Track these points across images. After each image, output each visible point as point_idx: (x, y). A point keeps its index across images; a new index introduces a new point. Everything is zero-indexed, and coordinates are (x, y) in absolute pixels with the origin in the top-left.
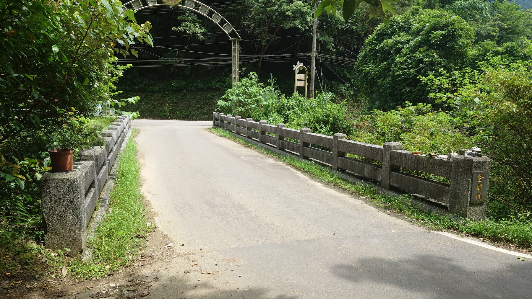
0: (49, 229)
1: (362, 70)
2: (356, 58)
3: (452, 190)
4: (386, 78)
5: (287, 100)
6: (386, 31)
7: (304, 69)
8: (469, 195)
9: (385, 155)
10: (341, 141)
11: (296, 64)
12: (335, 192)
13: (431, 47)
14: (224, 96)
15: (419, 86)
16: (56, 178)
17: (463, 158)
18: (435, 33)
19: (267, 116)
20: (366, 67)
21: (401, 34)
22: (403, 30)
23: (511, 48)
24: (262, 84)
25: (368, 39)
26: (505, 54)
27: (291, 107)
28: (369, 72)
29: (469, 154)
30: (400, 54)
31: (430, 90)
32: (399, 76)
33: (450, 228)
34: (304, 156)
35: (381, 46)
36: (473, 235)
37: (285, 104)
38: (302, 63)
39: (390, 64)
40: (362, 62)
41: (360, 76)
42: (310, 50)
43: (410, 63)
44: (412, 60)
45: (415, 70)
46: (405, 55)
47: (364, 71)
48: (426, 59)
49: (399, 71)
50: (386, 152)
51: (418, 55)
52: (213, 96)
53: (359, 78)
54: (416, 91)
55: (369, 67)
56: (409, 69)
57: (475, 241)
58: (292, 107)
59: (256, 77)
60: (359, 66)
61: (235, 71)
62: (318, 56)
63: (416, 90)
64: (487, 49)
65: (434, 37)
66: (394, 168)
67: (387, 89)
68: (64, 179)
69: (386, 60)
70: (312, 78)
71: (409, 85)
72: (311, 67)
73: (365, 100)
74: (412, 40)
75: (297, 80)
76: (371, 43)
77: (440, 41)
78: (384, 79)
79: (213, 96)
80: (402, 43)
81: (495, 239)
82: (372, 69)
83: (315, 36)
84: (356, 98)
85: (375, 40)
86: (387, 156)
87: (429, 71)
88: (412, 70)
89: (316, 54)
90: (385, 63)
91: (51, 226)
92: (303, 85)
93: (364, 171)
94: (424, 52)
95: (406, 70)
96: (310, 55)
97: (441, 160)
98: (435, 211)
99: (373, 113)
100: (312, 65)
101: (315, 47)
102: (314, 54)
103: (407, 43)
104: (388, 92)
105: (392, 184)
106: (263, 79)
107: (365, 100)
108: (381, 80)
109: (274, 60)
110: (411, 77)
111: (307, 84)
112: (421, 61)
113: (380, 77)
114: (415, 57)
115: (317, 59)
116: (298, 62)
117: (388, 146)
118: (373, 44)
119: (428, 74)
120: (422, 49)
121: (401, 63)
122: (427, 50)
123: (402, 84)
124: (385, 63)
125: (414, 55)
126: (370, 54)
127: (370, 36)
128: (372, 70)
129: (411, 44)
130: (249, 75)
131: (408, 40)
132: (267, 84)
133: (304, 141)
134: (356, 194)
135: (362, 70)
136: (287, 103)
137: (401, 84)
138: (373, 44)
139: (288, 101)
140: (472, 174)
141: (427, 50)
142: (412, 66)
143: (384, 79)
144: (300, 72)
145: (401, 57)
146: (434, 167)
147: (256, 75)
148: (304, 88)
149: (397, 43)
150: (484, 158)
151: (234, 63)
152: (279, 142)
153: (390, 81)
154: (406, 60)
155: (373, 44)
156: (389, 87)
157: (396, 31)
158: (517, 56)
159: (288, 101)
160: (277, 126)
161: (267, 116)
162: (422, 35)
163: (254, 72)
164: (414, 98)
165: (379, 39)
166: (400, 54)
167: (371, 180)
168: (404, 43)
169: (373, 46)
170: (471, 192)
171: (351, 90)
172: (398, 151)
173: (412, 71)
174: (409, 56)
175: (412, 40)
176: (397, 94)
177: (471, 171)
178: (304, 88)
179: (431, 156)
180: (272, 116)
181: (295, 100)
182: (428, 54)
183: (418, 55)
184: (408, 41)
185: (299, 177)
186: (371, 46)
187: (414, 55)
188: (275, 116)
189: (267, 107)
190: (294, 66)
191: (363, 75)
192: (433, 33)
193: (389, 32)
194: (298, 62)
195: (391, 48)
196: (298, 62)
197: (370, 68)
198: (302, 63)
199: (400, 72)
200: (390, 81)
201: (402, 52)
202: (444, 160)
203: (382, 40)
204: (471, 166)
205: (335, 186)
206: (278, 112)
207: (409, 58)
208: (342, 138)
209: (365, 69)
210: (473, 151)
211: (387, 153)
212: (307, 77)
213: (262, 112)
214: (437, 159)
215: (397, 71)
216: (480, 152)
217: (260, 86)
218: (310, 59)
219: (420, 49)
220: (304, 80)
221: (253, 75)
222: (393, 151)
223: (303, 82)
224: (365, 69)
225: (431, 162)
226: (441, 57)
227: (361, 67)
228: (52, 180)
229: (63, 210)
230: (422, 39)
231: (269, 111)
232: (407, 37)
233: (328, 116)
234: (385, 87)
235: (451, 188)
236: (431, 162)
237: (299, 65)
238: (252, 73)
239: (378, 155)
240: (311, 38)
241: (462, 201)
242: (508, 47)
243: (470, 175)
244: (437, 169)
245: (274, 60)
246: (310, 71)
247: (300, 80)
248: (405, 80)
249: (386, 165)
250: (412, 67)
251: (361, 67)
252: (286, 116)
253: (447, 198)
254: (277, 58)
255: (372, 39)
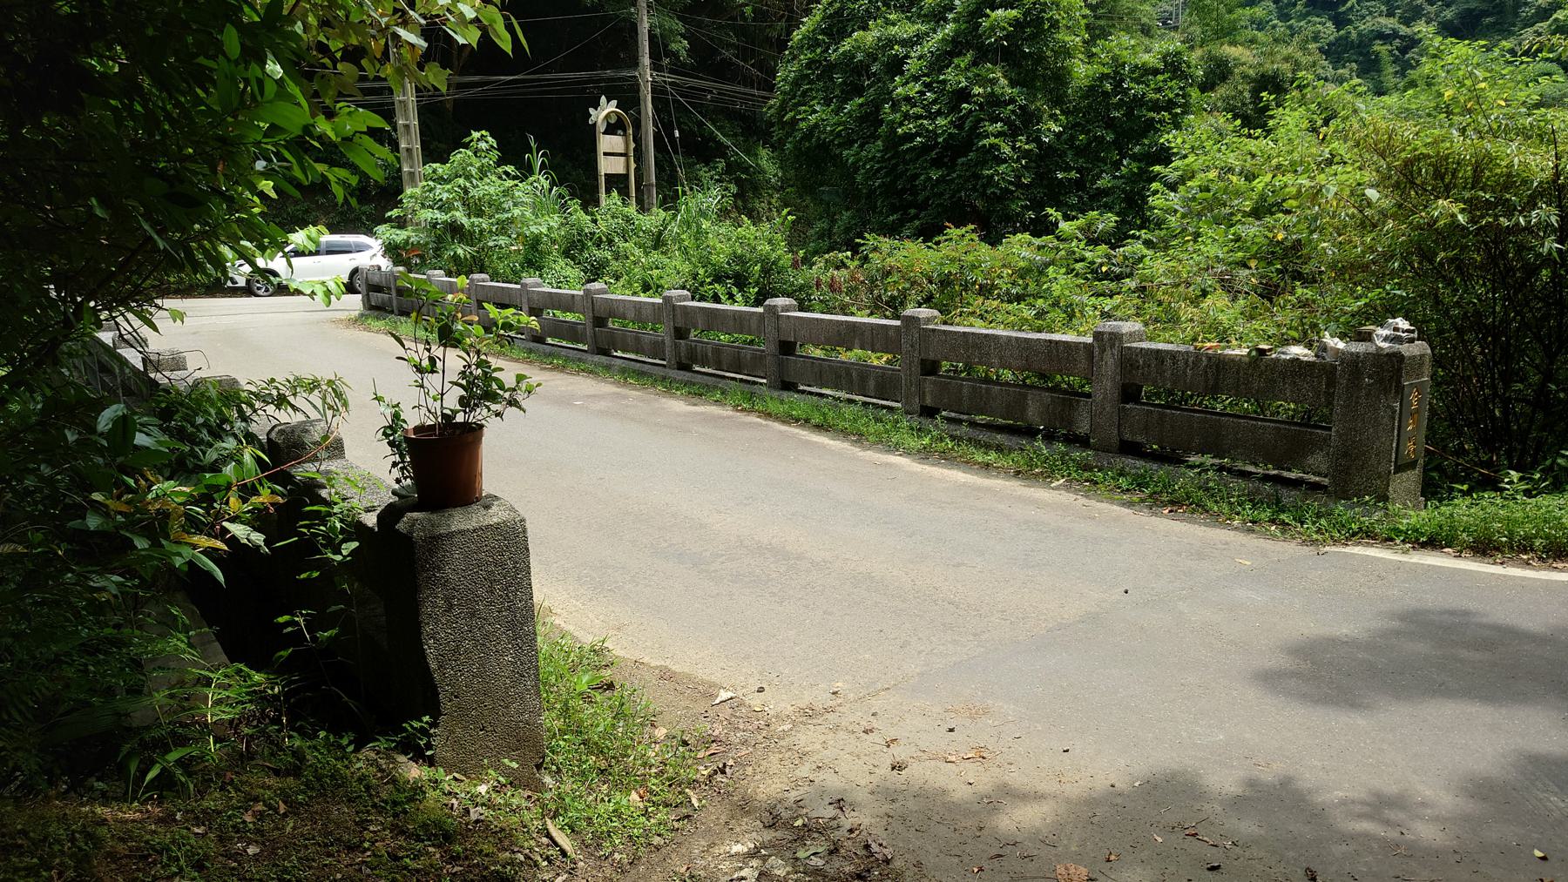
0: (446, 705)
1: (794, 122)
2: (771, 88)
3: (1340, 436)
4: (868, 143)
5: (589, 218)
6: (853, 7)
7: (620, 121)
8: (1394, 445)
9: (1102, 360)
10: (934, 330)
11: (596, 106)
12: (968, 476)
13: (985, 55)
14: (394, 213)
15: (962, 164)
16: (463, 527)
17: (1372, 349)
18: (993, 15)
19: (540, 268)
20: (805, 111)
21: (892, 17)
22: (895, 5)
23: (1174, 56)
24: (510, 169)
25: (799, 28)
26: (1163, 73)
27: (604, 239)
28: (816, 126)
29: (1386, 339)
30: (902, 73)
31: (992, 175)
32: (909, 137)
33: (1368, 535)
34: (783, 382)
35: (841, 50)
36: (1423, 545)
37: (587, 231)
38: (614, 102)
39: (877, 106)
40: (790, 99)
41: (790, 140)
42: (634, 63)
43: (935, 102)
44: (935, 93)
45: (949, 119)
46: (916, 79)
47: (803, 125)
48: (977, 90)
49: (906, 122)
50: (1103, 351)
51: (953, 77)
52: (307, 211)
53: (788, 145)
54: (955, 179)
55: (815, 112)
56: (932, 117)
57: (1441, 559)
58: (607, 238)
59: (492, 146)
60: (783, 109)
61: (407, 127)
62: (658, 79)
63: (955, 175)
64: (1120, 61)
65: (992, 28)
66: (1129, 393)
67: (872, 174)
68: (488, 527)
69: (859, 91)
70: (647, 146)
71: (936, 163)
72: (639, 113)
73: (770, 209)
74: (927, 34)
75: (605, 154)
76: (811, 42)
77: (1006, 38)
78: (862, 146)
79: (307, 211)
80: (904, 43)
81: (1484, 547)
82: (824, 116)
83: (645, 18)
84: (745, 202)
85: (823, 32)
86: (1110, 361)
87: (987, 124)
88: (941, 121)
89: (651, 75)
90: (861, 101)
91: (452, 693)
92: (621, 170)
93: (1024, 409)
94: (967, 69)
95: (925, 122)
96: (635, 77)
97: (1296, 361)
98: (1288, 496)
99: (864, 244)
100: (642, 107)
101: (647, 50)
102: (646, 74)
103: (916, 43)
104: (877, 184)
105: (1127, 436)
106: (512, 154)
107: (770, 209)
108: (854, 148)
109: (525, 90)
110: (940, 140)
111: (633, 166)
112: (963, 95)
113: (849, 143)
114: (944, 82)
115: (658, 91)
116: (603, 99)
117: (1110, 334)
118: (819, 45)
119: (984, 131)
120: (963, 62)
121: (908, 99)
122: (975, 63)
123: (917, 159)
124: (861, 101)
125: (942, 77)
126: (813, 74)
127: (805, 20)
128: (824, 120)
129: (931, 44)
130: (467, 140)
131: (917, 35)
132: (526, 171)
133: (782, 338)
134: (1044, 474)
135: (794, 122)
136: (591, 225)
137: (914, 161)
138: (817, 44)
139: (595, 221)
140: (1400, 390)
141: (975, 63)
142: (940, 108)
143: (862, 146)
144: (611, 130)
145: (907, 83)
146: (1275, 382)
147: (490, 139)
148: (626, 177)
149: (890, 42)
150: (1420, 348)
151: (400, 102)
152: (676, 346)
153: (878, 151)
154: (922, 93)
155: (817, 44)
156: (878, 170)
157: (878, 8)
158: (1191, 76)
159: (595, 221)
160: (664, 298)
161: (540, 268)
162: (955, 20)
163: (484, 132)
164: (951, 198)
165: (832, 31)
166: (902, 73)
167: (1059, 430)
168: (908, 43)
169: (819, 51)
170: (1399, 435)
171: (730, 182)
172: (1145, 345)
173: (943, 123)
174: (928, 80)
175: (927, 34)
176: (904, 191)
177: (1399, 382)
178: (626, 177)
179: (1262, 352)
180: (552, 269)
181: (613, 217)
182: (979, 75)
183: (953, 77)
184: (919, 38)
185: (824, 446)
186: (814, 51)
187: (942, 77)
188: (562, 267)
189: (534, 243)
190: (591, 110)
191: (799, 135)
192: (988, 16)
193: (859, 11)
194: (603, 99)
195: (873, 58)
196: (603, 97)
197: (817, 114)
198: (614, 102)
199: (911, 126)
200: (878, 151)
201: (908, 70)
202: (1306, 359)
203: (843, 34)
204: (1399, 370)
205: (946, 458)
206: (566, 254)
207: (928, 86)
208: (929, 320)
209: (803, 119)
210: (1396, 329)
211: (1108, 352)
212: (632, 145)
213: (521, 257)
214: (1285, 360)
215: (901, 124)
216: (1412, 332)
217: (506, 173)
218: (635, 88)
219: (956, 61)
220: (625, 155)
221: (483, 140)
222: (1130, 348)
223: (622, 159)
224: (803, 119)
225: (1263, 368)
226: (1012, 84)
227: (792, 114)
228: (451, 535)
229: (486, 636)
230: (957, 33)
231: (541, 253)
232: (916, 27)
233: (740, 259)
234: (868, 171)
235: (1338, 431)
236: (1263, 368)
237: (606, 110)
238: (476, 135)
239: (1076, 360)
240: (634, 28)
241: (1374, 460)
242: (1168, 54)
243: (1397, 392)
244: (1284, 385)
245: (525, 90)
246: (637, 125)
247: (611, 156)
248: (925, 149)
249: (1105, 387)
250: (939, 113)
251: (792, 114)
252: (593, 265)
253: (1318, 460)
254: (537, 86)
255: (813, 31)
